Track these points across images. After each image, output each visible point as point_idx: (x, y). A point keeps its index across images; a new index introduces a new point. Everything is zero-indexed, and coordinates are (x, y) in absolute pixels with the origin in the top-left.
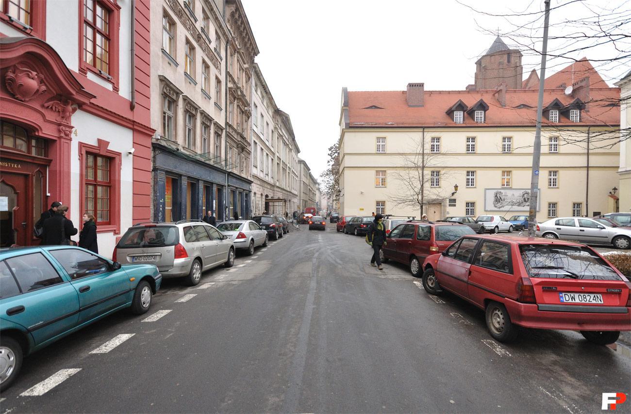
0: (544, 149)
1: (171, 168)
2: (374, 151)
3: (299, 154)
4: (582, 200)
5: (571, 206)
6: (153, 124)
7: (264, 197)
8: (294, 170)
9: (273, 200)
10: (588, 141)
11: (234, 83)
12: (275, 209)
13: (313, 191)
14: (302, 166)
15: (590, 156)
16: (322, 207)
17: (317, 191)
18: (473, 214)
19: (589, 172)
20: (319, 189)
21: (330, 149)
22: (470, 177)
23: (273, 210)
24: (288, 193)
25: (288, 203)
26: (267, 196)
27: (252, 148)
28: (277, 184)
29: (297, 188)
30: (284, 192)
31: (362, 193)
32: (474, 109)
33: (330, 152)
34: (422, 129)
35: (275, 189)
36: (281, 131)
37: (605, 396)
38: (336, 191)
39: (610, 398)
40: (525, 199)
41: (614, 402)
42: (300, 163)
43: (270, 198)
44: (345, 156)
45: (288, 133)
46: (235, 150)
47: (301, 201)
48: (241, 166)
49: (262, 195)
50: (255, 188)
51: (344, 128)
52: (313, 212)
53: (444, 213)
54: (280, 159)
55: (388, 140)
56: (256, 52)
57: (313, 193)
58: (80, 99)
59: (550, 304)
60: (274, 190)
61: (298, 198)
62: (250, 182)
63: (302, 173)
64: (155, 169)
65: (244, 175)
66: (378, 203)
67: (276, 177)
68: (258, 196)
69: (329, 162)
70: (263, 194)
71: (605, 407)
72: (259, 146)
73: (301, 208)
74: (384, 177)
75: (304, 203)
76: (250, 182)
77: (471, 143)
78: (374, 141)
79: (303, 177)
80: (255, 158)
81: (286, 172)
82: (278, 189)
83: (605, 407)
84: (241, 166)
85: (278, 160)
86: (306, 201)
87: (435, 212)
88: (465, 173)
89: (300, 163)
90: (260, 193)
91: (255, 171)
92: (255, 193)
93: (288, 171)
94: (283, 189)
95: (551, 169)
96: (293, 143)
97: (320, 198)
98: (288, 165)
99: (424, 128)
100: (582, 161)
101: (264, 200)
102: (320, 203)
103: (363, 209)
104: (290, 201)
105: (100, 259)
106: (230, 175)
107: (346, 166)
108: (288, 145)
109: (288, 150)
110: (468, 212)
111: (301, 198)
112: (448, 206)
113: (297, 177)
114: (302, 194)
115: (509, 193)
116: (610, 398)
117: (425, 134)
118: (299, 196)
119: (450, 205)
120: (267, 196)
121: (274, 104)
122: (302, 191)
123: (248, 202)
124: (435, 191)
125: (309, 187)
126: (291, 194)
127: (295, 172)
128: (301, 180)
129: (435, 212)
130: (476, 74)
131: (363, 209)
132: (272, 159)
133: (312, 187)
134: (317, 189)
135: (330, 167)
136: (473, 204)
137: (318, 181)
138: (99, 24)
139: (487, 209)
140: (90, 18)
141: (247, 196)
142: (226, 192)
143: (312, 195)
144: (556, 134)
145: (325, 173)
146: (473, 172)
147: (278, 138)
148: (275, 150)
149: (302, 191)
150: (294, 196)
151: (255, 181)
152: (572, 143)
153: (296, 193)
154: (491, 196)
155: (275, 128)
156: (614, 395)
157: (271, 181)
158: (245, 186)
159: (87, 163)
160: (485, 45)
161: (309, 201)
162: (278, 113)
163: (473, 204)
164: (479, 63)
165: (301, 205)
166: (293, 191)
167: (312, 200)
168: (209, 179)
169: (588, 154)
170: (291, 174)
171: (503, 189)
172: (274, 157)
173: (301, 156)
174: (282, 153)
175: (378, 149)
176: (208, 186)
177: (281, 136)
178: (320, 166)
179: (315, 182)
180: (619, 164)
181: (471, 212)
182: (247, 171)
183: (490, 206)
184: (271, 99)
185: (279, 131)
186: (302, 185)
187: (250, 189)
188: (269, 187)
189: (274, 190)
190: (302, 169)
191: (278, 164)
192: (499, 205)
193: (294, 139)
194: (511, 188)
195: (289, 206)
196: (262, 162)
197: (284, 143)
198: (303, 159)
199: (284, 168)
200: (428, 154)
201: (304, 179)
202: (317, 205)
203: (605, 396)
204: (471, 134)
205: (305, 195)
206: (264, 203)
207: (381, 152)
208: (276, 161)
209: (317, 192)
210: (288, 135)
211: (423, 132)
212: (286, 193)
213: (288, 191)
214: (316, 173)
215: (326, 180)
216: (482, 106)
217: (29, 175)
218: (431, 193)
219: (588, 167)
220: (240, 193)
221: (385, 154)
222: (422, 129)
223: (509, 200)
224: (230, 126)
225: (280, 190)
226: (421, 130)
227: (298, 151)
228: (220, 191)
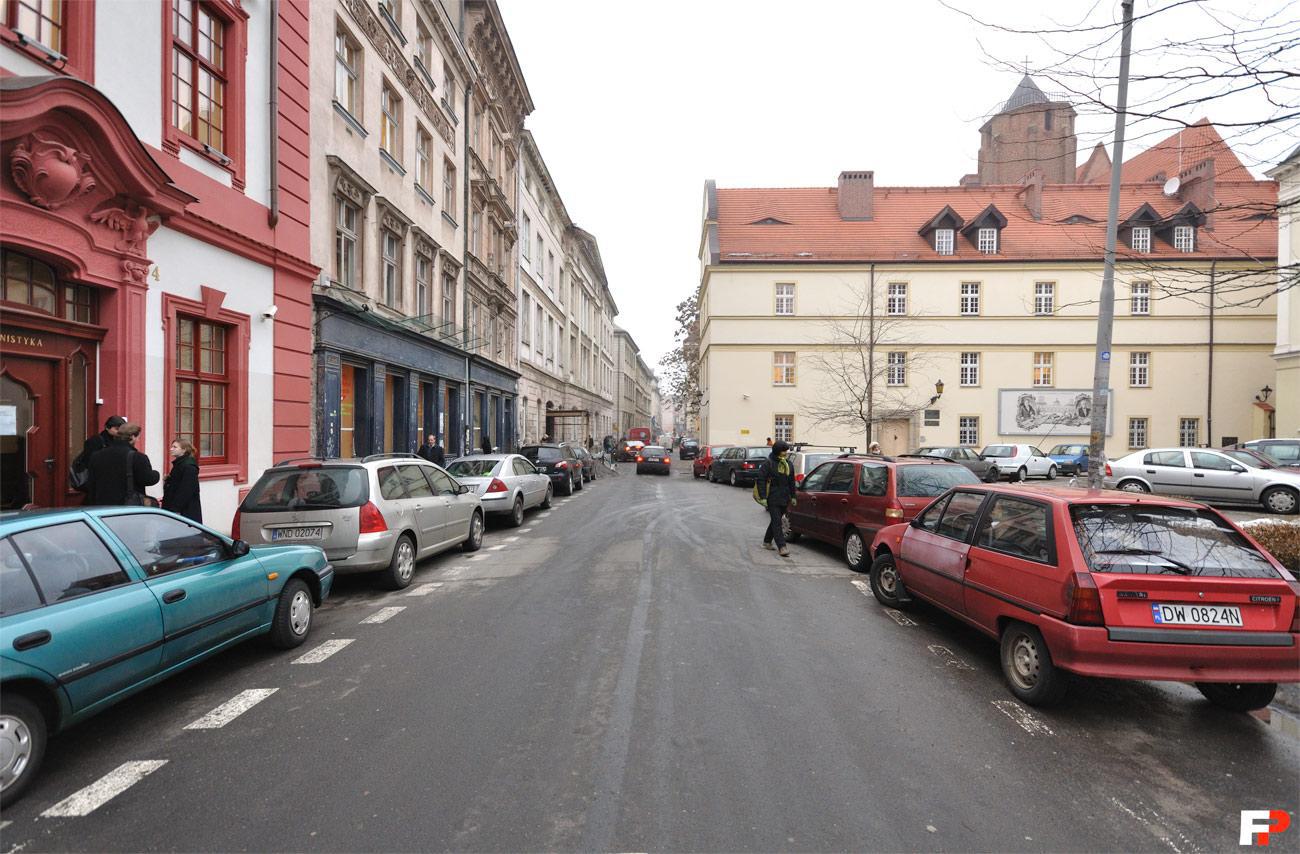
0: (1121, 308)
1: (352, 346)
2: (771, 311)
3: (615, 318)
4: (1200, 412)
5: (1177, 424)
6: (315, 255)
7: (544, 406)
8: (605, 352)
9: (562, 412)
10: (1212, 290)
11: (483, 170)
12: (567, 431)
13: (644, 395)
14: (623, 342)
15: (1215, 322)
16: (664, 427)
17: (653, 395)
18: (975, 442)
19: (1214, 354)
20: (657, 390)
21: (680, 308)
22: (969, 365)
23: (563, 434)
24: (594, 399)
25: (594, 420)
26: (550, 404)
27: (519, 306)
28: (572, 380)
29: (613, 388)
30: (585, 395)
31: (745, 398)
32: (977, 225)
33: (680, 314)
34: (870, 266)
35: (567, 389)
36: (579, 269)
37: (1247, 816)
38: (693, 395)
39: (1256, 822)
40: (1081, 411)
41: (1265, 829)
42: (619, 337)
43: (556, 408)
44: (712, 322)
45: (593, 275)
46: (485, 310)
47: (621, 414)
48: (497, 343)
49: (539, 402)
50: (525, 387)
51: (709, 263)
52: (646, 436)
53: (914, 439)
54: (577, 328)
55: (800, 289)
56: (528, 108)
57: (645, 398)
58: (164, 204)
59: (1134, 627)
60: (564, 393)
61: (614, 408)
62: (515, 376)
63: (623, 357)
64: (319, 349)
65: (502, 362)
66: (778, 419)
67: (568, 366)
68: (532, 403)
69: (677, 334)
70: (542, 400)
71: (1245, 839)
72: (534, 300)
73: (620, 428)
74: (792, 365)
75: (627, 418)
76: (515, 376)
77: (970, 295)
78: (771, 291)
79: (623, 364)
80: (526, 326)
81: (589, 355)
82: (572, 391)
83: (1245, 839)
84: (497, 343)
85: (572, 330)
86: (630, 415)
87: (896, 438)
88: (958, 356)
89: (619, 337)
90: (536, 399)
91: (525, 353)
92: (525, 399)
93: (593, 352)
94: (584, 391)
95: (1135, 350)
96: (604, 296)
97: (660, 409)
98: (594, 341)
99: (873, 264)
100: (1198, 332)
101: (543, 412)
102: (660, 419)
103: (748, 432)
104: (597, 414)
105: (206, 533)
106: (474, 360)
107: (712, 342)
108: (593, 298)
109: (593, 309)
110: (965, 437)
111: (621, 409)
112: (922, 424)
113: (613, 364)
114: (622, 400)
115: (1049, 398)
116: (1256, 822)
117: (876, 275)
118: (615, 403)
119: (927, 424)
120: (550, 404)
121: (564, 214)
122: (622, 393)
123: (510, 417)
125: (636, 386)
126: (600, 401)
127: (608, 356)
128: (621, 371)
129: (896, 438)
130: (980, 152)
131: (748, 432)
132: (561, 329)
133: (643, 385)
134: (653, 390)
135: (680, 346)
136: (974, 421)
137: (656, 374)
138: (204, 50)
139: (1004, 431)
141: (510, 403)
142: (466, 395)
143: (643, 403)
144: (1146, 276)
145: (671, 357)
146: (974, 355)
147: (572, 285)
148: (566, 310)
149: (622, 393)
150: (606, 404)
151: (526, 373)
152: (1179, 295)
153: (609, 397)
154: (1011, 404)
155: (567, 264)
156: (1265, 814)
157: (558, 374)
158: (506, 385)
160: (998, 93)
161: (637, 416)
162: (573, 233)
163: (974, 421)
164: (986, 130)
165: (621, 422)
166: (604, 395)
167: (643, 413)
168: (431, 369)
169: (1211, 318)
170: (599, 359)
171: (1036, 389)
172: (564, 325)
173: (620, 322)
174: (582, 315)
175: (779, 307)
176: (429, 384)
177: (580, 280)
178: (658, 342)
179: (649, 376)
180: (1275, 338)
181: (970, 437)
182: (509, 353)
183: (1010, 425)
184: (558, 205)
185: (576, 270)
186: (622, 381)
187: (515, 390)
188: (554, 386)
189: (564, 393)
190: (623, 349)
191: (572, 338)
192: (1028, 422)
193: (605, 288)
194: (1052, 389)
195: (595, 424)
196: (540, 335)
197: (585, 296)
198: (624, 327)
199: (584, 346)
200: (882, 318)
201: (626, 369)
202: (653, 422)
203: (1247, 816)
204: (971, 277)
205: (628, 402)
206: (544, 419)
207: (784, 313)
208: (569, 332)
209: (653, 397)
210: (594, 277)
211: (872, 272)
212: (590, 398)
213: (592, 395)
214: (651, 357)
215: (672, 370)
217: (60, 360)
218: (888, 399)
219: (1211, 345)
220: (495, 398)
221: (793, 318)
222: (870, 266)
223: (1049, 414)
224: (474, 260)
225: (576, 392)
226: (868, 268)
227: (614, 311)
228: (453, 393)
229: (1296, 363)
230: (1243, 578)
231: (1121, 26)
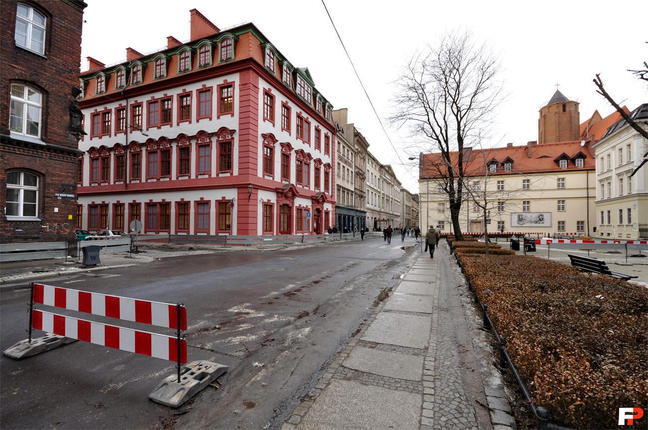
4: (584, 219)
5: (576, 223)
7: (373, 219)
8: (396, 199)
9: (380, 221)
10: (486, 201)
14: (405, 193)
15: (589, 190)
19: (589, 200)
26: (375, 218)
27: (366, 195)
28: (383, 210)
29: (400, 209)
30: (387, 215)
37: (622, 411)
39: (627, 413)
40: (540, 219)
41: (631, 417)
43: (377, 219)
46: (359, 198)
48: (361, 205)
50: (368, 215)
56: (367, 145)
62: (365, 212)
63: (405, 198)
64: (336, 214)
65: (362, 209)
67: (381, 206)
68: (370, 218)
71: (621, 422)
72: (370, 191)
75: (407, 221)
76: (365, 212)
77: (501, 184)
79: (405, 201)
80: (368, 198)
83: (621, 422)
84: (361, 205)
86: (409, 220)
91: (368, 206)
92: (368, 218)
93: (390, 200)
95: (559, 199)
98: (391, 196)
100: (584, 193)
101: (373, 221)
104: (392, 220)
105: (67, 338)
106: (357, 211)
111: (405, 218)
114: (405, 214)
115: (528, 215)
116: (627, 413)
122: (405, 212)
123: (364, 222)
124: (635, 203)
125: (412, 208)
130: (539, 120)
136: (563, 222)
138: (269, 103)
139: (513, 225)
140: (266, 102)
141: (364, 219)
142: (355, 218)
149: (405, 212)
152: (574, 180)
153: (399, 214)
154: (515, 218)
155: (381, 176)
156: (631, 410)
158: (363, 215)
160: (546, 98)
163: (563, 222)
164: (541, 111)
166: (395, 213)
168: (349, 214)
169: (588, 188)
171: (524, 212)
174: (387, 190)
175: (559, 185)
176: (349, 216)
180: (595, 194)
182: (364, 207)
183: (515, 223)
184: (377, 162)
185: (384, 177)
186: (405, 208)
188: (377, 213)
191: (383, 197)
192: (521, 223)
193: (395, 178)
194: (529, 212)
196: (372, 200)
199: (387, 199)
203: (622, 411)
204: (501, 179)
206: (373, 222)
208: (381, 196)
216: (509, 160)
219: (588, 197)
220: (361, 218)
223: (528, 220)
224: (356, 189)
225: (384, 214)
226: (586, 172)
227: (400, 184)
228: (353, 218)
229: (647, 198)
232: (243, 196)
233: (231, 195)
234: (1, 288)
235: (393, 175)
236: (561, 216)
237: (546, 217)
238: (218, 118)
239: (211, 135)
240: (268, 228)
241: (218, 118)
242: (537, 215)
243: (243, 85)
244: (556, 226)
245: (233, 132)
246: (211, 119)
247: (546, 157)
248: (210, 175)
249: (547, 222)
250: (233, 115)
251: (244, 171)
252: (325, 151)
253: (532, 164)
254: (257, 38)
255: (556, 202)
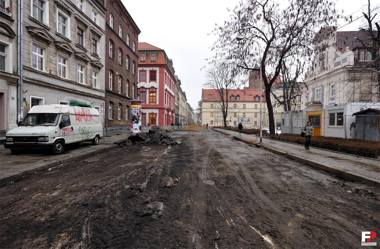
1: (96, 146)
2: (254, 108)
11: (246, 66)
14: (187, 105)
20: (193, 113)
37: (364, 233)
38: (200, 115)
39: (366, 235)
41: (369, 237)
78: (254, 105)
116: (366, 235)
136: (256, 122)
156: (369, 233)
159: (283, 78)
161: (190, 119)
163: (256, 122)
167: (190, 119)
173: (187, 102)
175: (255, 107)
193: (186, 98)
201: (188, 110)
203: (364, 233)
216: (238, 96)
226: (293, 128)
230: (59, 79)
231: (216, 88)
232: (161, 112)
233: (156, 111)
234: (1, 140)
235: (185, 97)
236: (255, 119)
237: (251, 119)
238: (150, 82)
239: (281, 138)
240: (165, 124)
241: (150, 82)
242: (248, 119)
243: (160, 72)
244: (254, 123)
245: (157, 88)
246: (146, 82)
247: (251, 95)
248: (146, 104)
249: (251, 122)
250: (156, 82)
251: (161, 103)
252: (10, 22)
253: (247, 98)
254: (92, 5)
255: (254, 114)
